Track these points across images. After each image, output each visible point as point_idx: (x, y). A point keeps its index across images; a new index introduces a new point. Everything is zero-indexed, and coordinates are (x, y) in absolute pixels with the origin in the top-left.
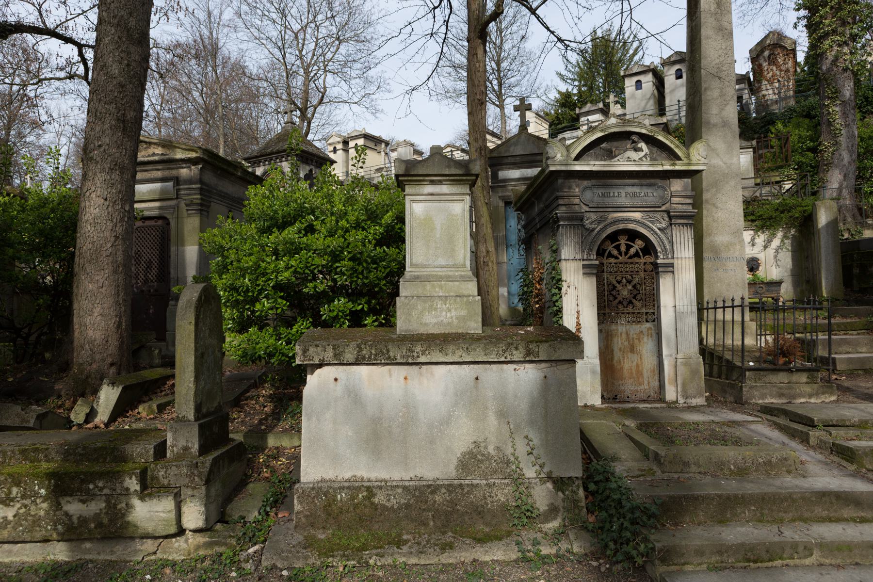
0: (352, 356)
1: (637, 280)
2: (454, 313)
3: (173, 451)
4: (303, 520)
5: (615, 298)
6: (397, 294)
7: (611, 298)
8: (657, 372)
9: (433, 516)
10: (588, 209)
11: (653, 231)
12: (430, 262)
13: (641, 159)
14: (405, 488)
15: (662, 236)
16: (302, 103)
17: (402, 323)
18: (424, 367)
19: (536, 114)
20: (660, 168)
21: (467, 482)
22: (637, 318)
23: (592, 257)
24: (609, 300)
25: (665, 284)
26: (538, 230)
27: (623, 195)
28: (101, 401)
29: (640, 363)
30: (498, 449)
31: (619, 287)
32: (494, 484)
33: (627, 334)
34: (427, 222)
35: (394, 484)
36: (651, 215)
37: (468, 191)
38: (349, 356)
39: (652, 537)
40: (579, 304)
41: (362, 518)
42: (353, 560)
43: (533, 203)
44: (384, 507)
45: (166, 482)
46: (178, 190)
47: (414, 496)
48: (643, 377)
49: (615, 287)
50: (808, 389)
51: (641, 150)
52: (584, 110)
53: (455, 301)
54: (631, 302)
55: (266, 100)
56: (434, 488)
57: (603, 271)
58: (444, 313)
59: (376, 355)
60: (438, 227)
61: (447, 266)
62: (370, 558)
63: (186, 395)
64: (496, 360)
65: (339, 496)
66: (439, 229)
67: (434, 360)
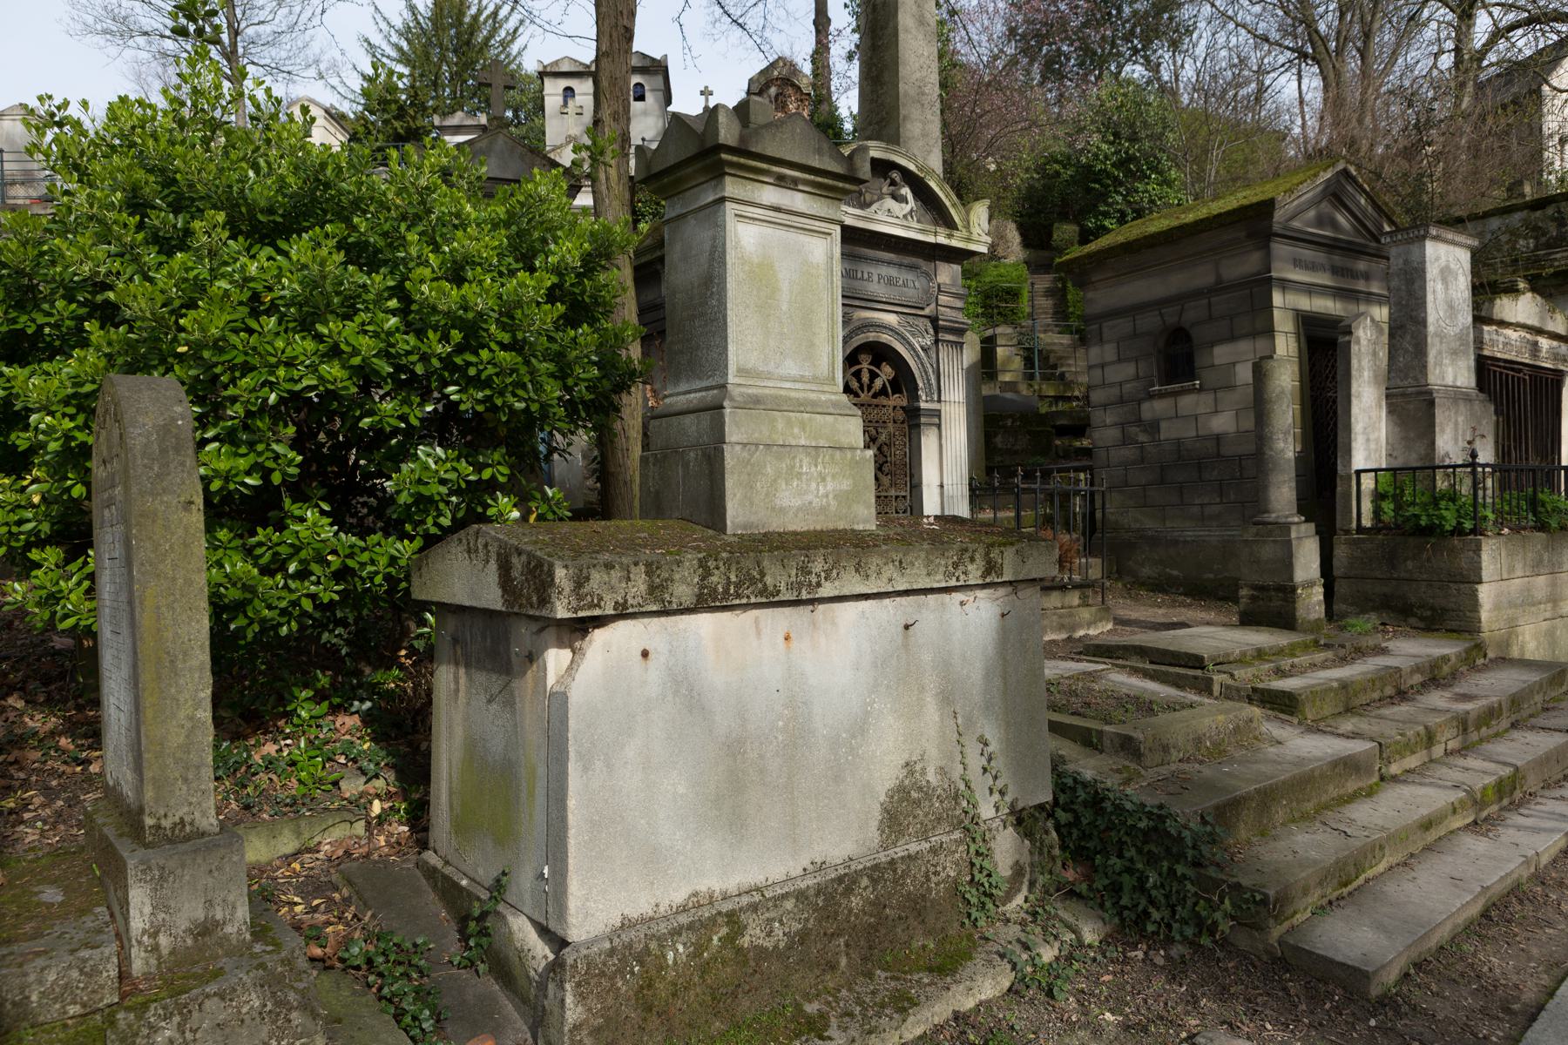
1: (883, 438)
3: (156, 948)
9: (847, 945)
11: (914, 350)
12: (771, 367)
14: (800, 895)
17: (739, 512)
18: (821, 607)
19: (327, 111)
20: (931, 239)
25: (928, 443)
27: (875, 278)
30: (942, 771)
34: (762, 274)
36: (910, 319)
38: (683, 592)
44: (761, 953)
50: (1086, 614)
51: (903, 200)
53: (832, 457)
56: (847, 882)
58: (814, 485)
59: (738, 585)
60: (785, 286)
61: (802, 380)
63: (186, 748)
64: (944, 585)
67: (846, 592)
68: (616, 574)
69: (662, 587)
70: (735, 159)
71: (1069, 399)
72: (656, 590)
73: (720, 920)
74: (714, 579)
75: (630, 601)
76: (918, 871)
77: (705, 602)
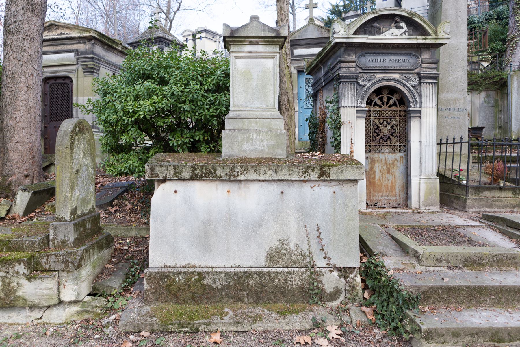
0: (188, 174)
1: (394, 122)
2: (265, 143)
3: (54, 243)
4: (151, 295)
5: (378, 135)
6: (223, 128)
7: (375, 135)
8: (405, 187)
9: (247, 294)
10: (361, 71)
11: (408, 87)
13: (401, 35)
14: (227, 274)
15: (414, 91)
16: (167, 10)
21: (273, 270)
22: (393, 150)
23: (363, 105)
24: (373, 136)
25: (414, 125)
26: (323, 87)
28: (17, 202)
29: (394, 181)
31: (381, 127)
32: (294, 271)
33: (386, 160)
35: (219, 270)
36: (407, 75)
37: (278, 50)
38: (186, 174)
39: (417, 320)
40: (354, 136)
41: (194, 293)
42: (187, 327)
43: (321, 68)
44: (211, 288)
45: (47, 267)
46: (78, 59)
47: (234, 279)
48: (395, 191)
49: (378, 127)
52: (347, 15)
54: (389, 138)
55: (145, 8)
56: (248, 275)
57: (370, 116)
58: (258, 143)
59: (206, 174)
62: (200, 326)
65: (177, 279)
66: (256, 87)
67: (250, 178)
68: (163, 169)
69: (179, 173)
70: (231, 39)
71: (361, 107)
72: (177, 174)
73: (195, 273)
74: (197, 172)
75: (168, 176)
76: (281, 277)
77: (193, 178)
